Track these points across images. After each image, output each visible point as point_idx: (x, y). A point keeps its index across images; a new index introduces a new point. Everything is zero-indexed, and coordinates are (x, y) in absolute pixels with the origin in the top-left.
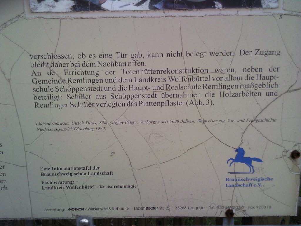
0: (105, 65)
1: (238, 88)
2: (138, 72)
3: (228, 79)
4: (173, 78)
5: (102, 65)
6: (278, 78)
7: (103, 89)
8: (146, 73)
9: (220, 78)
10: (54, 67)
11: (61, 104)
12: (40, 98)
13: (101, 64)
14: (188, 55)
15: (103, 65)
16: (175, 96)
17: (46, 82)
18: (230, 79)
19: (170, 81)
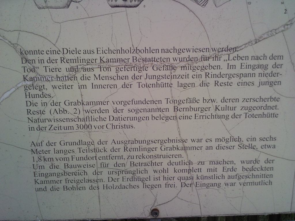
0: (35, 122)
1: (235, 68)
2: (154, 85)
4: (89, 111)
5: (32, 122)
8: (162, 86)
11: (141, 117)
13: (30, 119)
14: (153, 118)
15: (33, 122)
16: (185, 110)
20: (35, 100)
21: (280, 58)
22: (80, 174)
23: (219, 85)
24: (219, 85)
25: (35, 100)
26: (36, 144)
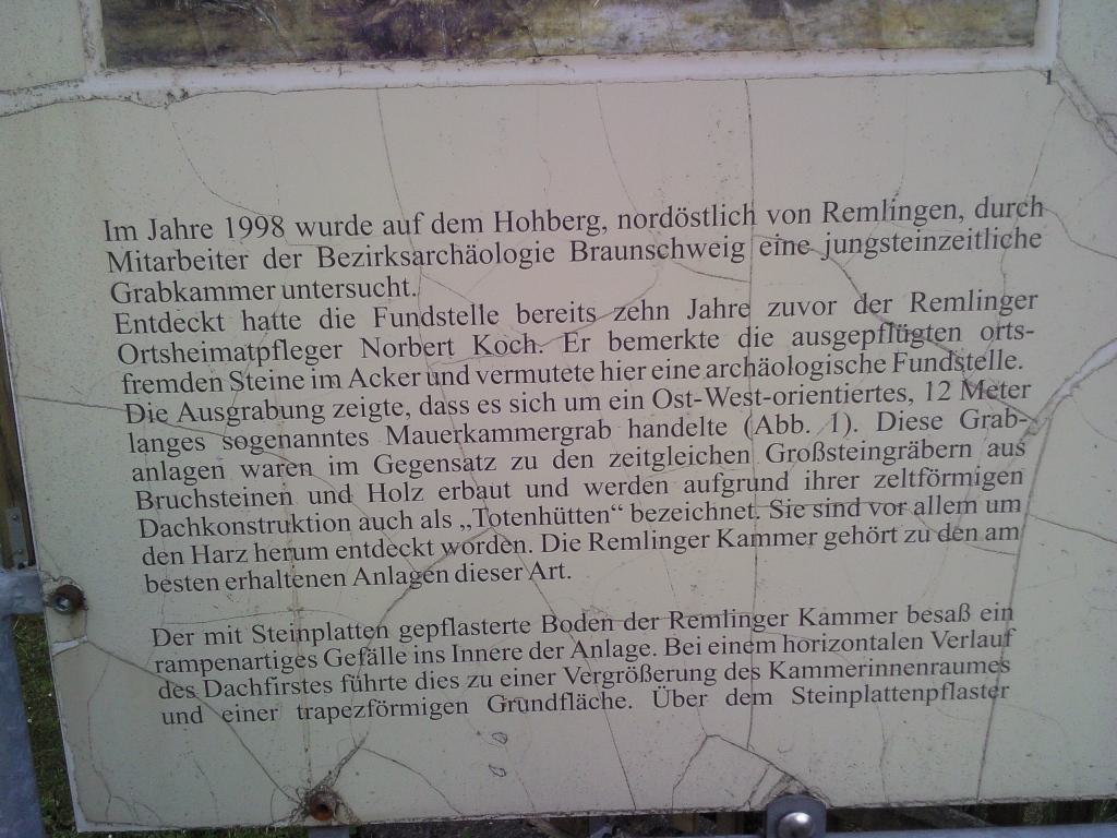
3: (379, 660)
6: (1032, 332)
7: (560, 405)
9: (827, 306)
10: (430, 413)
12: (861, 396)
17: (244, 295)
18: (935, 510)
19: (713, 404)
20: (158, 401)
21: (987, 305)
22: (154, 417)
23: (927, 307)
24: (927, 307)
25: (158, 401)
26: (196, 414)
